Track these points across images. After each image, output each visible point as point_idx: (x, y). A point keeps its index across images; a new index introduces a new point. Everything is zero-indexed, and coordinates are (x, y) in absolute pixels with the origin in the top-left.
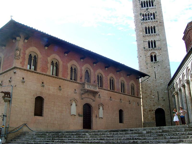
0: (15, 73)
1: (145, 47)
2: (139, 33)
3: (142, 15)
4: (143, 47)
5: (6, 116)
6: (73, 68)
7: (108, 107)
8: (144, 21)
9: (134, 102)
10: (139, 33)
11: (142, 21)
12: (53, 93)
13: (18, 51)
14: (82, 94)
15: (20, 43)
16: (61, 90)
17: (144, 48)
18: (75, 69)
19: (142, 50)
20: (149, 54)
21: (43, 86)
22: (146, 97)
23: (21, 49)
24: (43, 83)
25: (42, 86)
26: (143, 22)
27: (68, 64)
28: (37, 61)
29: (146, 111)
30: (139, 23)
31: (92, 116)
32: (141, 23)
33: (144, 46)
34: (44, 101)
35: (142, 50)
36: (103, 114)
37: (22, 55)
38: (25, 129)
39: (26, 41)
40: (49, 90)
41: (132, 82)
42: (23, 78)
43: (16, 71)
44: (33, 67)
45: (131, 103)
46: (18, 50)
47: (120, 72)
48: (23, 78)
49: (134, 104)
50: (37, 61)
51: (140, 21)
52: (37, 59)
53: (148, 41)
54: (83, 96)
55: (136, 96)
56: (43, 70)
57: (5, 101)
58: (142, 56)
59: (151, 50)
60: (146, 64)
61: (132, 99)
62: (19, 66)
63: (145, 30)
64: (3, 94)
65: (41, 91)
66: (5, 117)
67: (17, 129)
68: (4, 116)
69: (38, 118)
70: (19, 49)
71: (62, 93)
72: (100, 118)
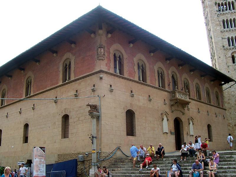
0: (101, 78)
1: (224, 45)
2: (215, 27)
3: (217, 5)
4: (222, 45)
5: (96, 137)
6: (117, 56)
7: (197, 121)
8: (221, 12)
9: (221, 114)
10: (215, 27)
11: (218, 13)
12: (143, 104)
13: (102, 48)
14: (172, 105)
15: (102, 38)
16: (133, 97)
17: (223, 47)
18: (119, 57)
19: (221, 49)
20: (229, 54)
21: (132, 96)
22: (231, 109)
23: (105, 46)
24: (132, 92)
25: (131, 95)
26: (220, 14)
27: (134, 58)
28: (123, 62)
29: (231, 126)
30: (214, 15)
31: (183, 134)
32: (217, 15)
33: (223, 44)
34: (135, 116)
35: (221, 49)
36: (193, 130)
37: (106, 54)
38: (119, 154)
39: (110, 35)
40: (139, 100)
41: (216, 89)
42: (111, 86)
43: (102, 76)
44: (118, 71)
45: (201, 112)
46: (102, 47)
47: (214, 81)
48: (111, 86)
49: (220, 117)
50: (122, 62)
51: (215, 13)
52: (122, 60)
53: (227, 37)
54: (173, 108)
55: (221, 107)
56: (130, 74)
57: (93, 117)
58: (221, 57)
59: (233, 49)
60: (227, 67)
61: (218, 110)
62: (105, 69)
63: (222, 24)
64: (89, 109)
65: (131, 103)
66: (95, 139)
67: (111, 155)
68: (93, 137)
69: (131, 139)
70: (103, 46)
71: (152, 105)
72: (190, 136)
